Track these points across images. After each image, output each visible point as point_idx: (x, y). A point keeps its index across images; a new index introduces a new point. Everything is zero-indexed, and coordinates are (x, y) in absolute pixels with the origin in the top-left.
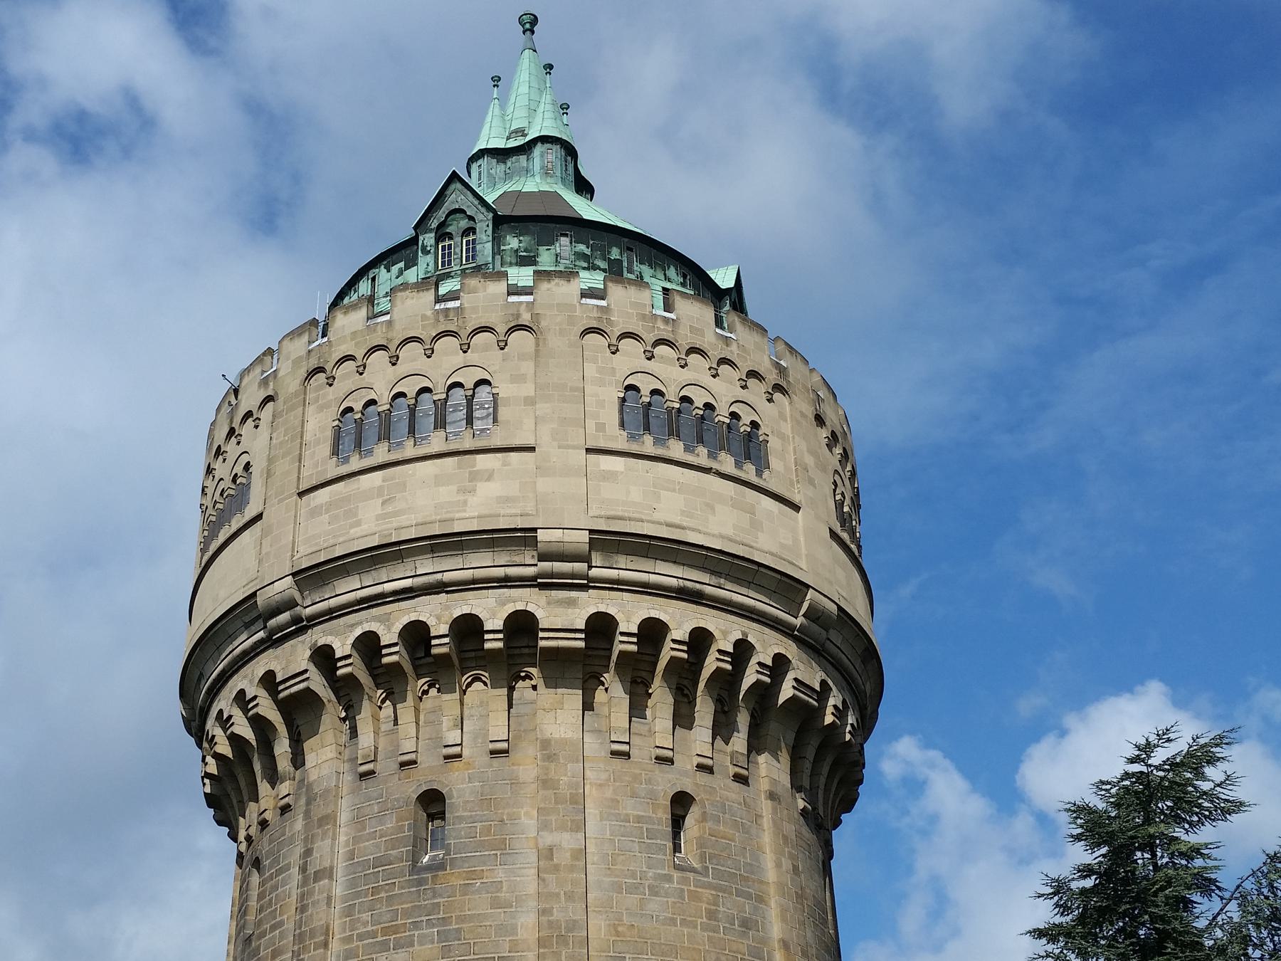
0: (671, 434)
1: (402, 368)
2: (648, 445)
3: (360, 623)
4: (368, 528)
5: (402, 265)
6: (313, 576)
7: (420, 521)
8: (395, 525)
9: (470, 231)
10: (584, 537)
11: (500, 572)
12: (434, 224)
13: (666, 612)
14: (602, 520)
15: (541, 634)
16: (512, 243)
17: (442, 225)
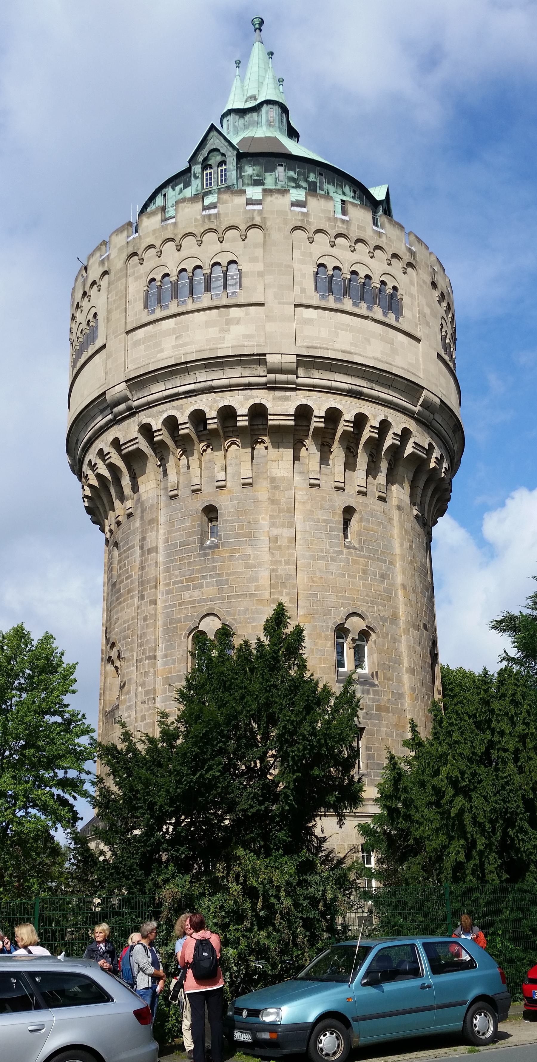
2: (331, 302)
3: (166, 410)
4: (167, 355)
5: (181, 186)
6: (138, 382)
7: (198, 349)
8: (183, 352)
10: (294, 359)
11: (245, 380)
12: (201, 159)
13: (341, 404)
14: (304, 349)
15: (270, 417)
16: (249, 170)
17: (206, 159)
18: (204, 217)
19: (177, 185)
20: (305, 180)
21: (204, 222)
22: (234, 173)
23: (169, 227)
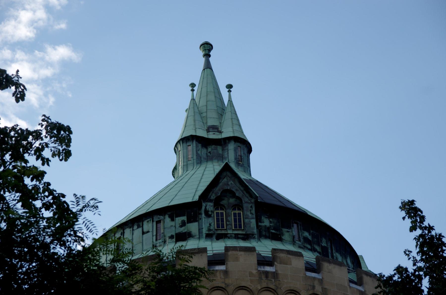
5: (185, 218)
9: (239, 206)
12: (213, 197)
16: (266, 222)
18: (260, 272)
20: (319, 245)
21: (261, 278)
22: (253, 221)
23: (218, 274)
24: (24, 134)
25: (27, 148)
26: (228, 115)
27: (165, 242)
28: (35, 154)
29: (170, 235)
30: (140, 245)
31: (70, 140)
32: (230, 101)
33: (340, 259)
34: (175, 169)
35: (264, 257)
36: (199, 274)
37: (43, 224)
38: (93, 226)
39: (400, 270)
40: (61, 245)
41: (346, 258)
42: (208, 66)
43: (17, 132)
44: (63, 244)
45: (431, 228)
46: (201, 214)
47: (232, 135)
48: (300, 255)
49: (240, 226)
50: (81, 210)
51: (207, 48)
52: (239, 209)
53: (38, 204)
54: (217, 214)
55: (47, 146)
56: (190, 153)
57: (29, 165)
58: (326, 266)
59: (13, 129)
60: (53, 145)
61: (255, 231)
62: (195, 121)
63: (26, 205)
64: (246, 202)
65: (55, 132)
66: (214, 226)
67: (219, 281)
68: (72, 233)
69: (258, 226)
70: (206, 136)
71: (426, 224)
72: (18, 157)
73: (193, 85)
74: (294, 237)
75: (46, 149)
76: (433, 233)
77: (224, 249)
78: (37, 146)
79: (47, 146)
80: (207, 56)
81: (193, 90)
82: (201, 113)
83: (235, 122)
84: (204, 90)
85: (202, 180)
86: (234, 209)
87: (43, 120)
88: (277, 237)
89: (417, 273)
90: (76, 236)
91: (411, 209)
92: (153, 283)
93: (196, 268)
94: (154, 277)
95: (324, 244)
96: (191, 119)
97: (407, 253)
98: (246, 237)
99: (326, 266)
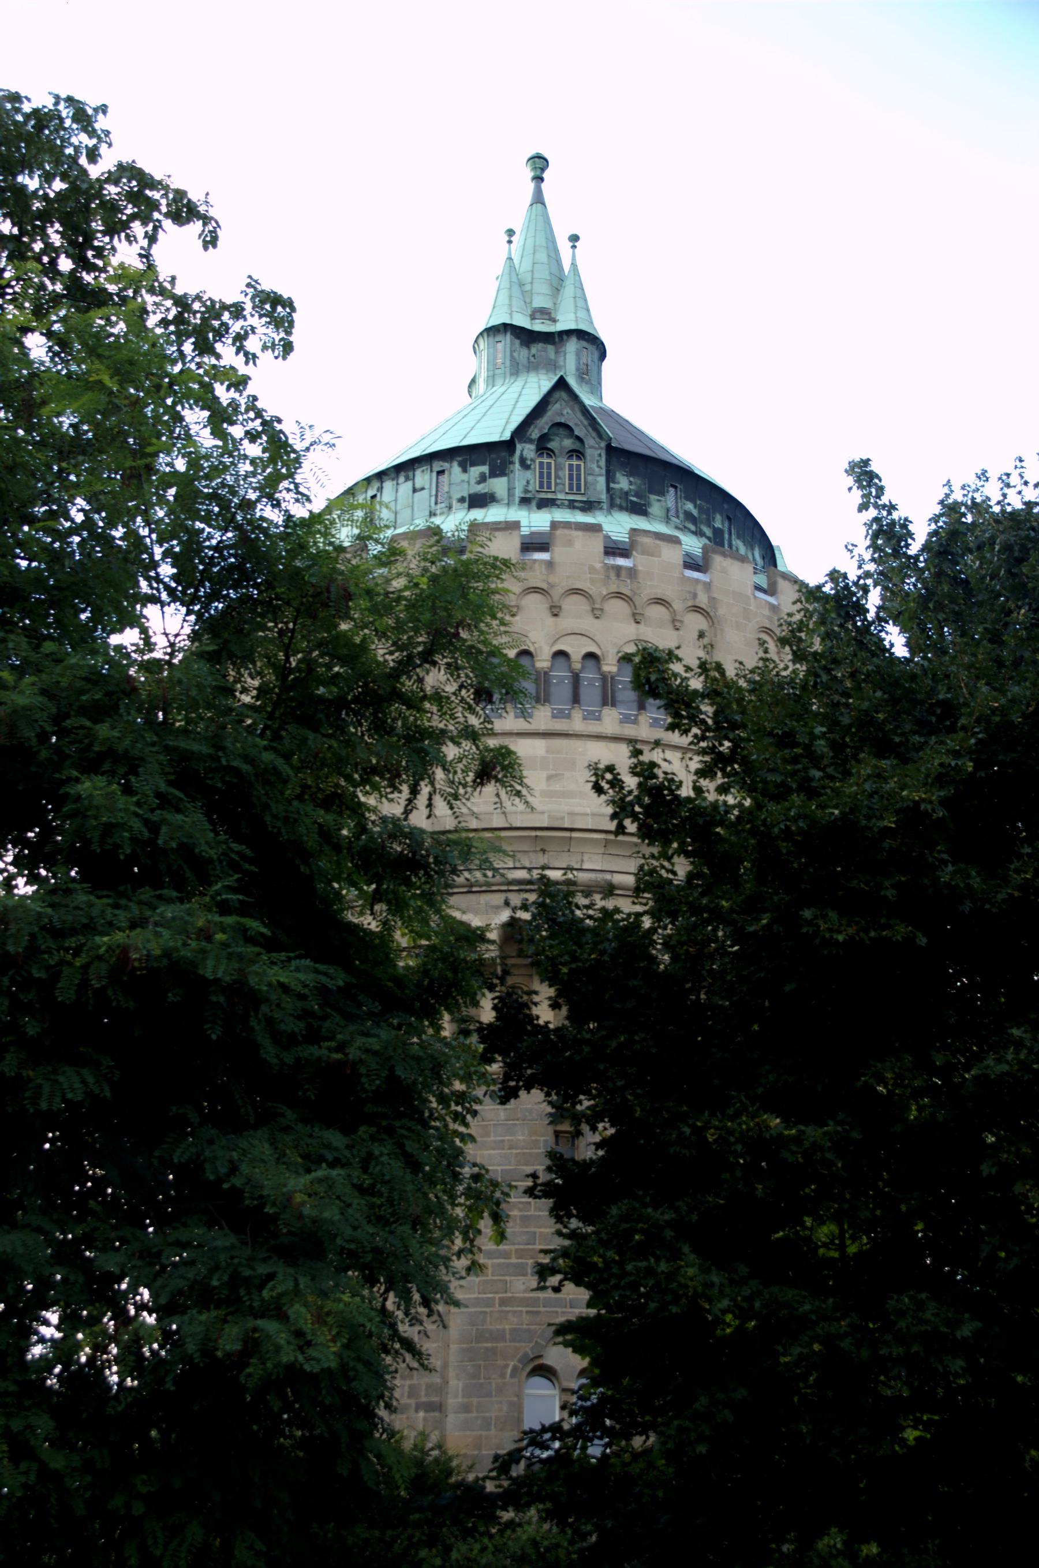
0: (604, 703)
1: (566, 623)
5: (485, 469)
8: (566, 808)
9: (577, 453)
12: (535, 433)
16: (623, 483)
17: (544, 439)
19: (473, 465)
20: (709, 526)
21: (608, 577)
22: (602, 480)
23: (537, 566)
24: (214, 310)
25: (221, 333)
26: (568, 291)
27: (450, 507)
28: (233, 344)
29: (459, 496)
30: (409, 511)
31: (291, 323)
32: (574, 265)
33: (742, 550)
34: (473, 381)
35: (615, 542)
36: (501, 569)
37: (245, 467)
38: (322, 480)
39: (835, 576)
40: (273, 506)
41: (753, 549)
42: (538, 199)
43: (204, 304)
44: (277, 505)
45: (892, 508)
46: (512, 463)
47: (573, 327)
48: (677, 541)
49: (579, 488)
50: (308, 449)
51: (539, 164)
52: (579, 458)
53: (237, 431)
54: (541, 464)
55: (254, 333)
56: (500, 355)
57: (222, 363)
58: (718, 561)
59: (198, 298)
60: (264, 330)
61: (604, 497)
62: (510, 297)
63: (218, 432)
64: (592, 447)
65: (268, 307)
66: (534, 485)
67: (536, 578)
68: (292, 487)
69: (608, 489)
70: (529, 327)
71: (884, 500)
72: (205, 348)
73: (511, 233)
74: (668, 510)
75: (251, 336)
76: (895, 515)
77: (548, 524)
78: (238, 330)
79: (254, 333)
80: (539, 179)
81: (510, 242)
82: (521, 285)
83: (581, 303)
84: (530, 242)
85: (519, 405)
86: (570, 457)
87: (249, 285)
88: (639, 509)
89: (862, 582)
90: (298, 493)
91: (864, 475)
92: (425, 580)
93: (496, 558)
94: (425, 570)
95: (718, 524)
96: (504, 293)
97: (850, 548)
98: (588, 507)
99: (718, 561)
